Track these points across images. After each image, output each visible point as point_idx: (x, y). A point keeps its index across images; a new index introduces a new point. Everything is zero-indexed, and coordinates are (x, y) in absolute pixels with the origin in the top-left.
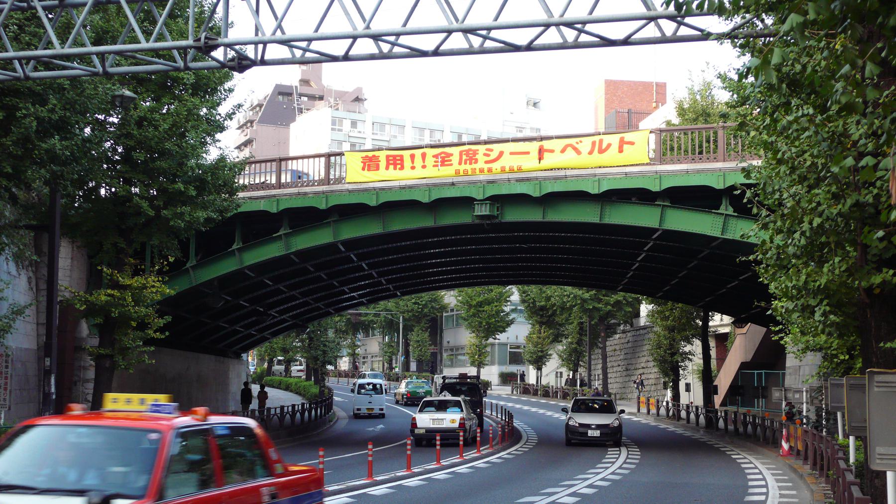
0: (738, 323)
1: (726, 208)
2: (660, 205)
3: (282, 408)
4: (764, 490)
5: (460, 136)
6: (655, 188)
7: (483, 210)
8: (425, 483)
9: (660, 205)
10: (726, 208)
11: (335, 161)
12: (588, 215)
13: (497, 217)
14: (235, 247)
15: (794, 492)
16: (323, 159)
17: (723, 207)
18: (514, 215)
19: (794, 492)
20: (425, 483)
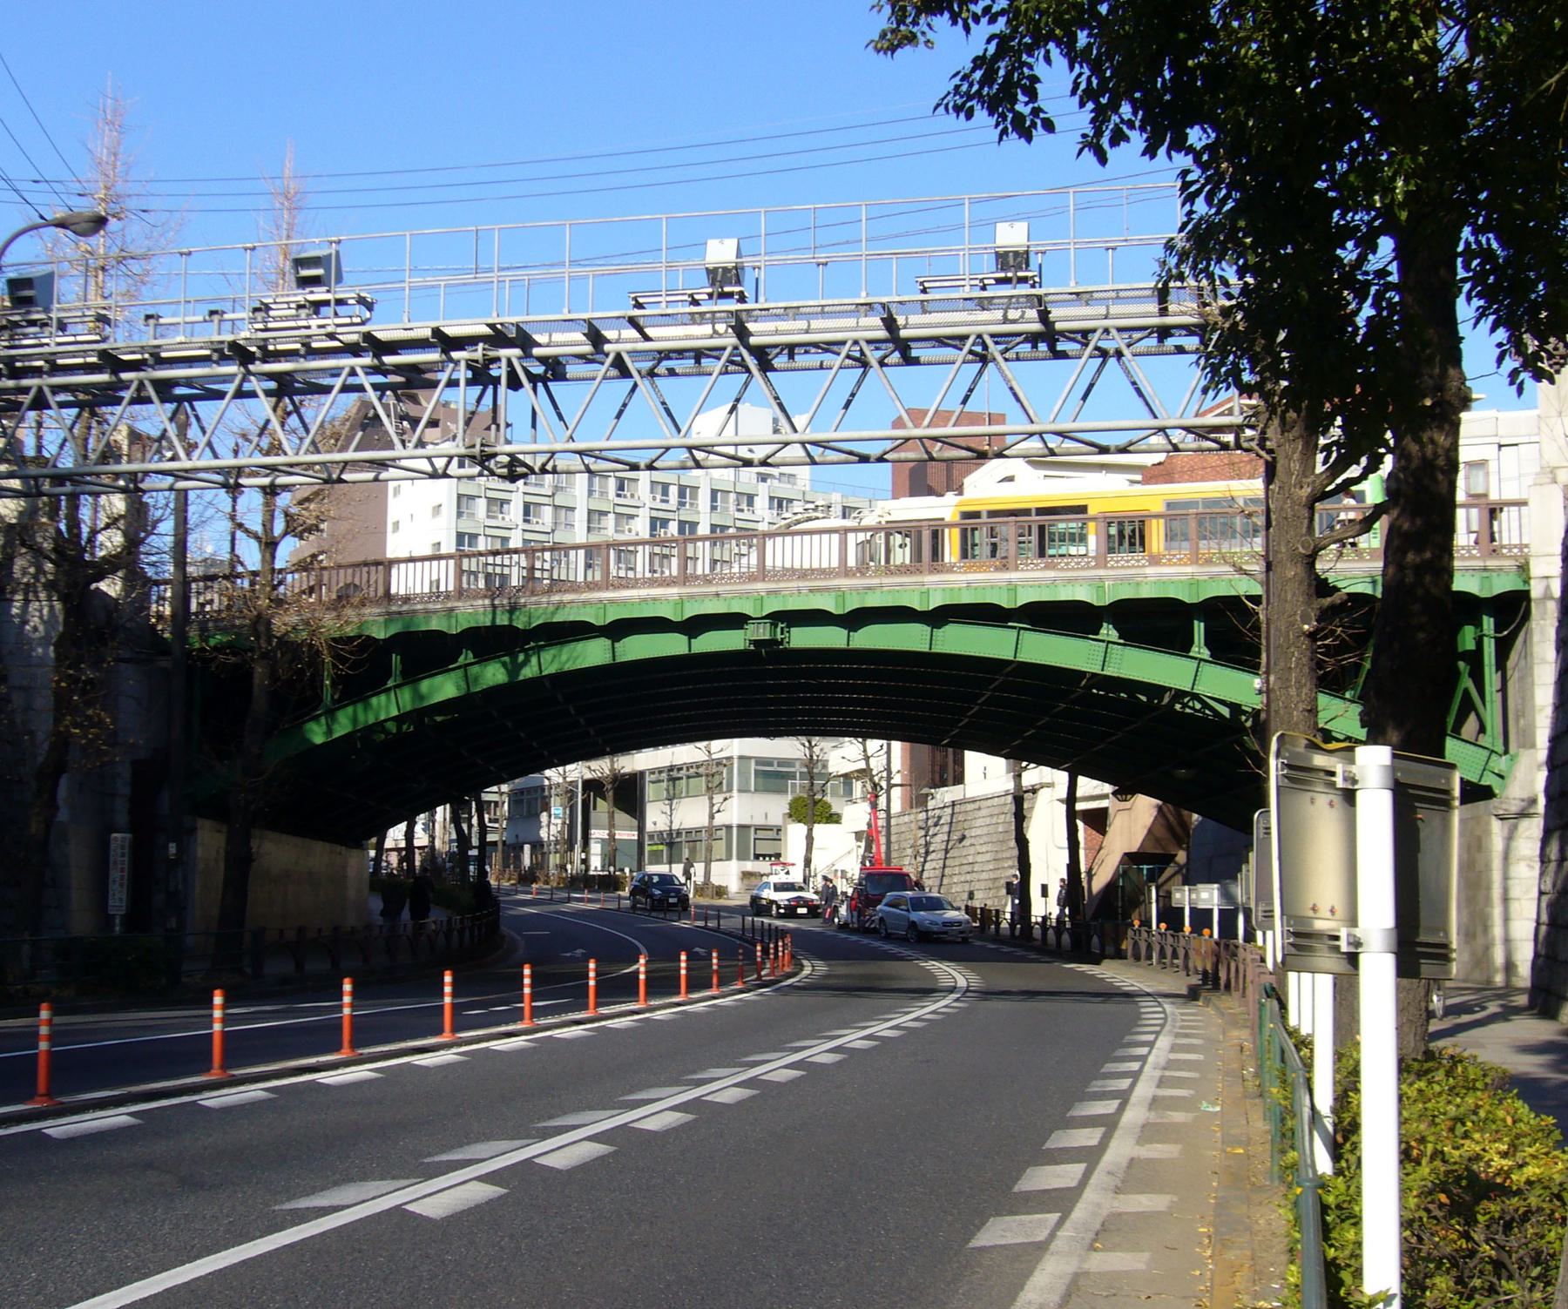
0: (1124, 791)
1: (1108, 632)
2: (1014, 628)
3: (300, 930)
4: (1162, 1016)
5: (505, 540)
6: (1006, 603)
7: (763, 632)
8: (379, 1075)
9: (1014, 628)
10: (1108, 632)
11: (354, 577)
12: (910, 638)
13: (781, 643)
14: (390, 683)
15: (1419, 949)
16: (835, 537)
17: (1103, 631)
18: (802, 638)
19: (1419, 949)
20: (379, 1075)
